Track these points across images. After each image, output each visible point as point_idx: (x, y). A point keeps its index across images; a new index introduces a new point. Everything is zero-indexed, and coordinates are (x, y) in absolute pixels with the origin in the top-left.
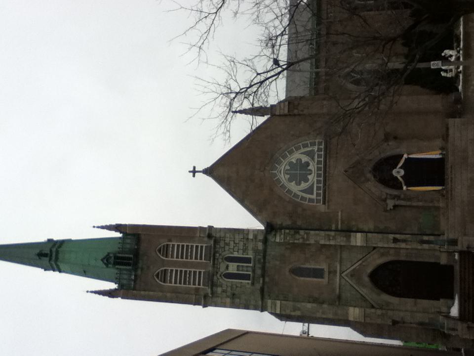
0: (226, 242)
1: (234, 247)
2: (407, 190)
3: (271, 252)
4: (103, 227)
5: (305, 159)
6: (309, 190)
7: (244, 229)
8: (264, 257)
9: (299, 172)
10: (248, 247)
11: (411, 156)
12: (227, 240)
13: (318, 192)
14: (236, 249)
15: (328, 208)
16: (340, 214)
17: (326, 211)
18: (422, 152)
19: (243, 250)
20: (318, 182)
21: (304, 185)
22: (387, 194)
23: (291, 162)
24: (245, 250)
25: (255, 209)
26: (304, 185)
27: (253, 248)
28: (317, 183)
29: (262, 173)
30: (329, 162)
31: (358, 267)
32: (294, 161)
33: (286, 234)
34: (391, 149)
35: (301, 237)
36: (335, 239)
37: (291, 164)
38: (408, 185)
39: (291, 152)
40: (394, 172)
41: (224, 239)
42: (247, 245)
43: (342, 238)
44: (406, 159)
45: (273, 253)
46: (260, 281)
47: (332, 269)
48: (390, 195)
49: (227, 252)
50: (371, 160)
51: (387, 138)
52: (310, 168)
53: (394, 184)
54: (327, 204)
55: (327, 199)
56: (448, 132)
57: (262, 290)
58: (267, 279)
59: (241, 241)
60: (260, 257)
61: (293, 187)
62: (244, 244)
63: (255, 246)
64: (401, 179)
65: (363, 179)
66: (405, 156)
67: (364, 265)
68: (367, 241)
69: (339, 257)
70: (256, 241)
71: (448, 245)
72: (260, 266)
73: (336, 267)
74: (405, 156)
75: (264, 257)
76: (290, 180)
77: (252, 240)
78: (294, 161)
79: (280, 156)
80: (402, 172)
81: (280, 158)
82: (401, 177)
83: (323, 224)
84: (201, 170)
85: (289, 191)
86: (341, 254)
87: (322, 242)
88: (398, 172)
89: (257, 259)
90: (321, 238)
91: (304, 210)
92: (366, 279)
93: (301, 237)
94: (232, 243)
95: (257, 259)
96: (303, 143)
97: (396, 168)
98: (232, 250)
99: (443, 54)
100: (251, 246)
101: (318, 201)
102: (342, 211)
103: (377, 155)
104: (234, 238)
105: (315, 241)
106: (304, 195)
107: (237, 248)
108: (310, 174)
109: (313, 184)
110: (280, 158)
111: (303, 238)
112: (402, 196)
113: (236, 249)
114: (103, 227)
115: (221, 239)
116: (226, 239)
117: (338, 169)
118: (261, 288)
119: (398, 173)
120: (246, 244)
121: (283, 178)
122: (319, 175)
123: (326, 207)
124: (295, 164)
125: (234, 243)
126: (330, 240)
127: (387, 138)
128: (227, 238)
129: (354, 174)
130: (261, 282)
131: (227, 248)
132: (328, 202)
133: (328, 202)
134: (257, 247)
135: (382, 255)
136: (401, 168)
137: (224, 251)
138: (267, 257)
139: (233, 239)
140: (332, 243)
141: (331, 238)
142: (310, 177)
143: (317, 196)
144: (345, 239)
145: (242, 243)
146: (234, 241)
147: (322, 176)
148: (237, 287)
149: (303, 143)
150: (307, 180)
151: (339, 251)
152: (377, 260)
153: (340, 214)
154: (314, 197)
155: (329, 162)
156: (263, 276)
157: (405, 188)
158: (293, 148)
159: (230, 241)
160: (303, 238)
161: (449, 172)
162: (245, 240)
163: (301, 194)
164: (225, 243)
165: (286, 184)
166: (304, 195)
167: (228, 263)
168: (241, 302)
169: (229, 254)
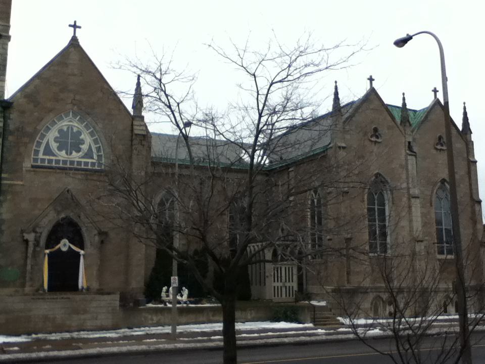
2: (45, 254)
5: (85, 147)
6: (48, 151)
16: (21, 183)
17: (24, 169)
20: (57, 162)
21: (54, 146)
22: (41, 233)
26: (54, 146)
29: (70, 101)
32: (82, 137)
34: (92, 237)
37: (79, 133)
39: (92, 134)
54: (32, 169)
55: (38, 170)
64: (57, 247)
65: (59, 209)
66: (82, 252)
78: (82, 137)
80: (64, 249)
81: (85, 123)
82: (60, 248)
84: (77, 35)
85: (48, 129)
96: (101, 148)
101: (35, 160)
108: (67, 153)
112: (38, 249)
119: (64, 245)
121: (64, 124)
122: (65, 162)
127: (103, 234)
129: (66, 199)
132: (34, 171)
142: (63, 153)
147: (57, 165)
150: (60, 149)
154: (41, 156)
157: (47, 251)
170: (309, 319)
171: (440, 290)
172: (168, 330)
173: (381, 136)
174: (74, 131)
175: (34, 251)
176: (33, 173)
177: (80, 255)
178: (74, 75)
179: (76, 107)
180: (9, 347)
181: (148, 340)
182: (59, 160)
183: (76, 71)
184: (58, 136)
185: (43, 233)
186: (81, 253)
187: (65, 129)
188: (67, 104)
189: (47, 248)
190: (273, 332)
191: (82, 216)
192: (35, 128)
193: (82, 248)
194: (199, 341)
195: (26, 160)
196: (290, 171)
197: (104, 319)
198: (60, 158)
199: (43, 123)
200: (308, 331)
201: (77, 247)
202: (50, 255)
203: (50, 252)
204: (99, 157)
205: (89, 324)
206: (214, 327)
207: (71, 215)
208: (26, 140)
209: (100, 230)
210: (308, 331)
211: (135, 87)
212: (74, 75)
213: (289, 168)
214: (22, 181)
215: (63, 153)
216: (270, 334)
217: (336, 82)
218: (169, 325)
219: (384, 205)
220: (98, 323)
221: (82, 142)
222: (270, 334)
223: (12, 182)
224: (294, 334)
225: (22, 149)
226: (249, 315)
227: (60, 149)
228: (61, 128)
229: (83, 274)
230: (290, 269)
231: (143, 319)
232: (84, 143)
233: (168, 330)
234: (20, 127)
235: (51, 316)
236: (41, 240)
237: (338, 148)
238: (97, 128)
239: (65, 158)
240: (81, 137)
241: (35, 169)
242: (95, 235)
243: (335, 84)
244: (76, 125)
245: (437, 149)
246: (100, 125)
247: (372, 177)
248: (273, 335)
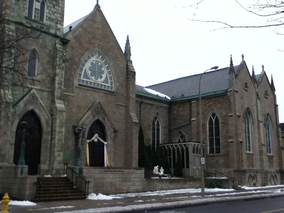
0: (56, 6)
1: (52, 11)
2: (87, 143)
3: (48, 39)
4: (272, 78)
5: (104, 76)
6: (86, 76)
7: (63, 22)
8: (45, 32)
9: (96, 71)
10: (52, 21)
11: (105, 146)
12: (56, 7)
13: (89, 82)
14: (51, 12)
15: (76, 87)
16: (72, 95)
17: (74, 85)
18: (108, 153)
19: (50, 17)
20: (91, 83)
21: (89, 72)
22: (85, 129)
23: (102, 67)
24: (50, 19)
25: (76, 34)
26: (89, 72)
27: (51, 25)
28: (90, 82)
29: (97, 45)
30: (103, 93)
31: (39, 102)
32: (103, 69)
33: (63, 53)
34: (109, 132)
35: (61, 63)
36: (59, 88)
37: (101, 66)
38: (89, 144)
39: (108, 68)
40: (96, 135)
41: (58, 5)
42: (53, 21)
43: (59, 93)
44: (103, 143)
45: (47, 40)
46: (28, 24)
47: (35, 82)
48: (85, 131)
49: (48, 4)
50: (105, 120)
51: (115, 131)
52: (99, 79)
53: (91, 135)
54: (79, 86)
55: (81, 87)
56: (138, 170)
57: (21, 24)
58: (29, 30)
59: (56, 18)
60: (45, 29)
61: (88, 65)
62: (54, 19)
63: (52, 28)
64: (92, 139)
65: (95, 114)
66: (105, 143)
67: (40, 107)
68: (60, 111)
69: (45, 89)
70: (56, 29)
71: (79, 168)
72: (39, 27)
73: (37, 86)
74: (105, 143)
75: (45, 32)
76: (92, 63)
77: (57, 27)
78: (103, 69)
79: (106, 60)
80: (96, 140)
81: (105, 60)
82: (93, 140)
83: (68, 83)
84: (99, 4)
85: (86, 61)
86: (46, 91)
87: (57, 78)
88: (96, 138)
89: (44, 26)
90: (60, 78)
91: (75, 70)
92: (30, 108)
93: (61, 63)
94: (55, 10)
95: (44, 26)
96: (112, 77)
97: (98, 136)
98: (50, 9)
99: (162, 168)
100: (53, 24)
101: (79, 80)
102: (74, 96)
103: (107, 126)
104: (58, 13)
105: (58, 73)
106: (83, 72)
107: (51, 13)
108: (95, 78)
109: (89, 79)
110: (105, 60)
111: (60, 65)
112: (84, 139)
113: (51, 12)
114: (272, 78)
115: (58, 3)
116: (57, 7)
117: (99, 98)
118: (24, 24)
119: (96, 138)
120: (54, 20)
121: (93, 59)
122: (94, 83)
123: (77, 86)
124: (101, 70)
125: (55, 12)
126: (59, 84)
127: (115, 131)
128: (58, 8)
129: (99, 109)
130: (28, 25)
131: (51, 5)
132: (79, 88)
133: (79, 88)
134: (52, 29)
135: (47, 122)
136: (98, 140)
137: (50, 3)
138: (45, 34)
139: (57, 12)
140: (57, 86)
141: (60, 86)
142: (93, 78)
143: (82, 80)
144: (59, 95)
145: (54, 18)
146: (56, 12)
147: (83, 84)
148: (24, 4)
149: (112, 77)
150: (92, 75)
151: (48, 90)
152: (44, 117)
153: (72, 95)
154: (82, 78)
155: (103, 93)
156: (32, 28)
157: (88, 141)
158: (110, 70)
159: (56, 9)
160: (60, 65)
161: (119, 170)
162: (56, 21)
163: (84, 69)
164: (55, 5)
165: (90, 61)
166: (83, 72)
167: (41, 2)
168: (13, 4)
169: (47, 5)
170: (231, 186)
171: (268, 172)
172: (199, 190)
173: (248, 88)
174: (99, 65)
175: (82, 140)
176: (78, 89)
177: (104, 145)
178: (99, 29)
179: (100, 49)
180: (138, 200)
181: (178, 198)
182: (92, 82)
183: (100, 27)
184: (91, 66)
185: (87, 129)
186: (104, 144)
187: (94, 62)
188: (96, 47)
189: (88, 139)
190: (228, 193)
191: (106, 120)
192: (79, 60)
193: (105, 141)
194: (218, 197)
195: (75, 80)
196: (192, 103)
197: (138, 186)
198: (92, 81)
199: (83, 57)
200: (230, 194)
201: (101, 139)
202: (89, 144)
203: (90, 142)
204: (111, 82)
205: (132, 188)
206: (175, 191)
207: (101, 119)
208: (75, 67)
209: (115, 129)
210: (230, 194)
211: (126, 42)
212: (99, 29)
213: (192, 101)
214: (73, 93)
215: (93, 78)
216: (226, 194)
217: (231, 55)
218: (200, 188)
219: (159, 126)
220: (135, 188)
221: (103, 72)
222: (226, 194)
223: (68, 94)
224: (235, 194)
225: (73, 73)
226: (197, 184)
227: (92, 75)
228: (92, 62)
229: (106, 158)
230: (200, 158)
231: (155, 186)
232: (103, 73)
233: (199, 190)
234: (72, 57)
235: (114, 183)
236: (276, 127)
237: (235, 92)
238: (110, 65)
239: (95, 81)
240: (102, 69)
241: (80, 86)
242: (112, 132)
243: (230, 56)
244: (100, 61)
245: (265, 97)
246: (112, 63)
247: (257, 102)
248: (237, 194)
